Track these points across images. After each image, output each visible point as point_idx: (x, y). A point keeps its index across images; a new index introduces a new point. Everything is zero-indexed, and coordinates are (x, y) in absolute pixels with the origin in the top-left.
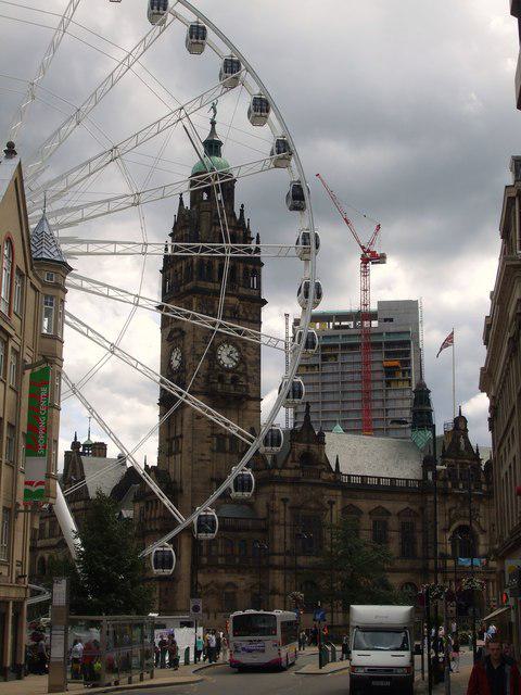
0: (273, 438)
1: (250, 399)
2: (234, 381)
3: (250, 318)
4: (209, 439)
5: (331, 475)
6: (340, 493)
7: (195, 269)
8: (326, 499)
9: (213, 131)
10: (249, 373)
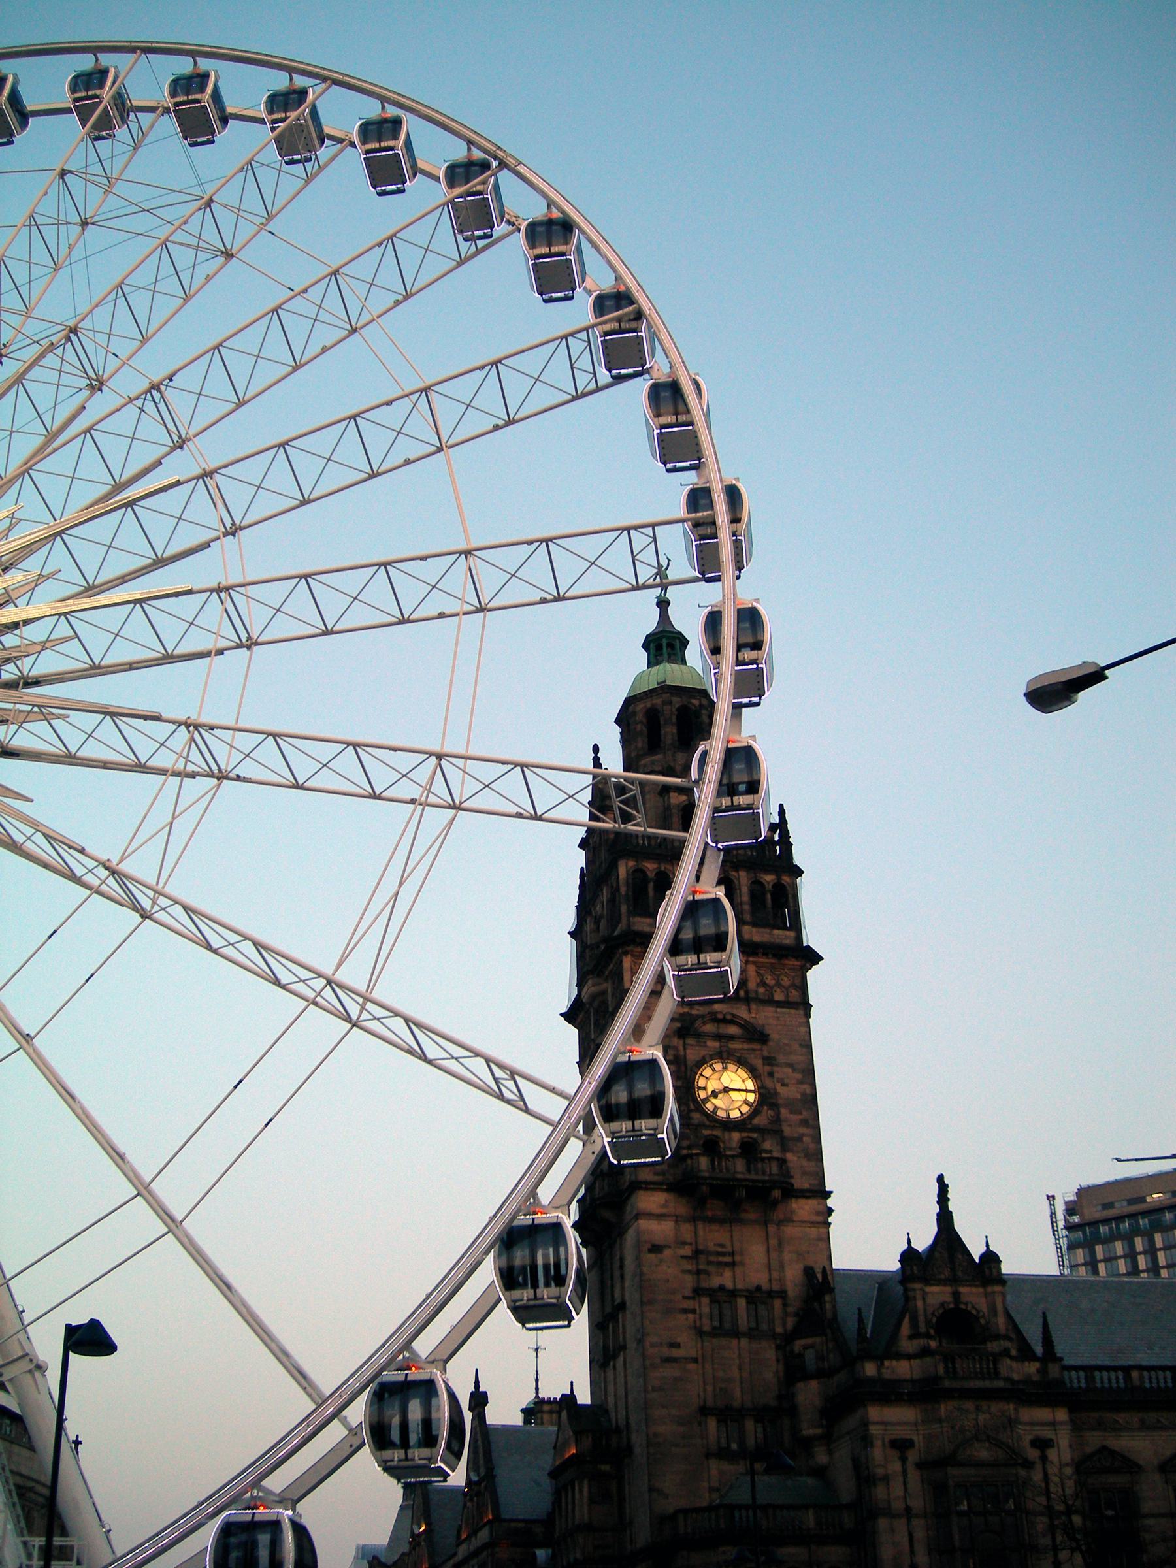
0: (683, 1083)
1: (790, 1192)
2: (749, 1150)
3: (779, 996)
4: (689, 1304)
5: (1032, 1368)
6: (1062, 1415)
7: (623, 890)
8: (1025, 1436)
9: (664, 617)
10: (787, 1131)
